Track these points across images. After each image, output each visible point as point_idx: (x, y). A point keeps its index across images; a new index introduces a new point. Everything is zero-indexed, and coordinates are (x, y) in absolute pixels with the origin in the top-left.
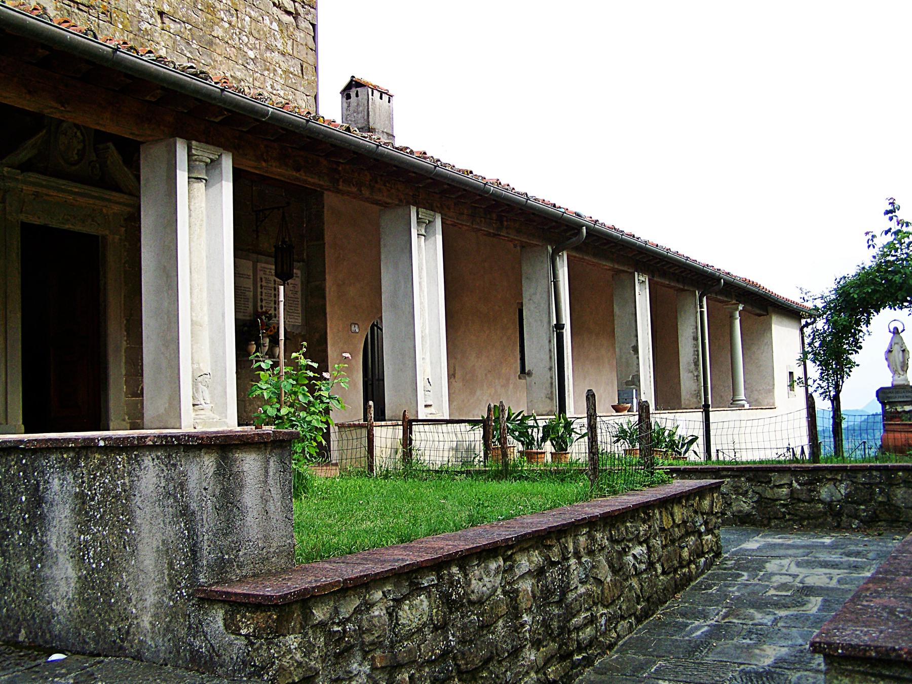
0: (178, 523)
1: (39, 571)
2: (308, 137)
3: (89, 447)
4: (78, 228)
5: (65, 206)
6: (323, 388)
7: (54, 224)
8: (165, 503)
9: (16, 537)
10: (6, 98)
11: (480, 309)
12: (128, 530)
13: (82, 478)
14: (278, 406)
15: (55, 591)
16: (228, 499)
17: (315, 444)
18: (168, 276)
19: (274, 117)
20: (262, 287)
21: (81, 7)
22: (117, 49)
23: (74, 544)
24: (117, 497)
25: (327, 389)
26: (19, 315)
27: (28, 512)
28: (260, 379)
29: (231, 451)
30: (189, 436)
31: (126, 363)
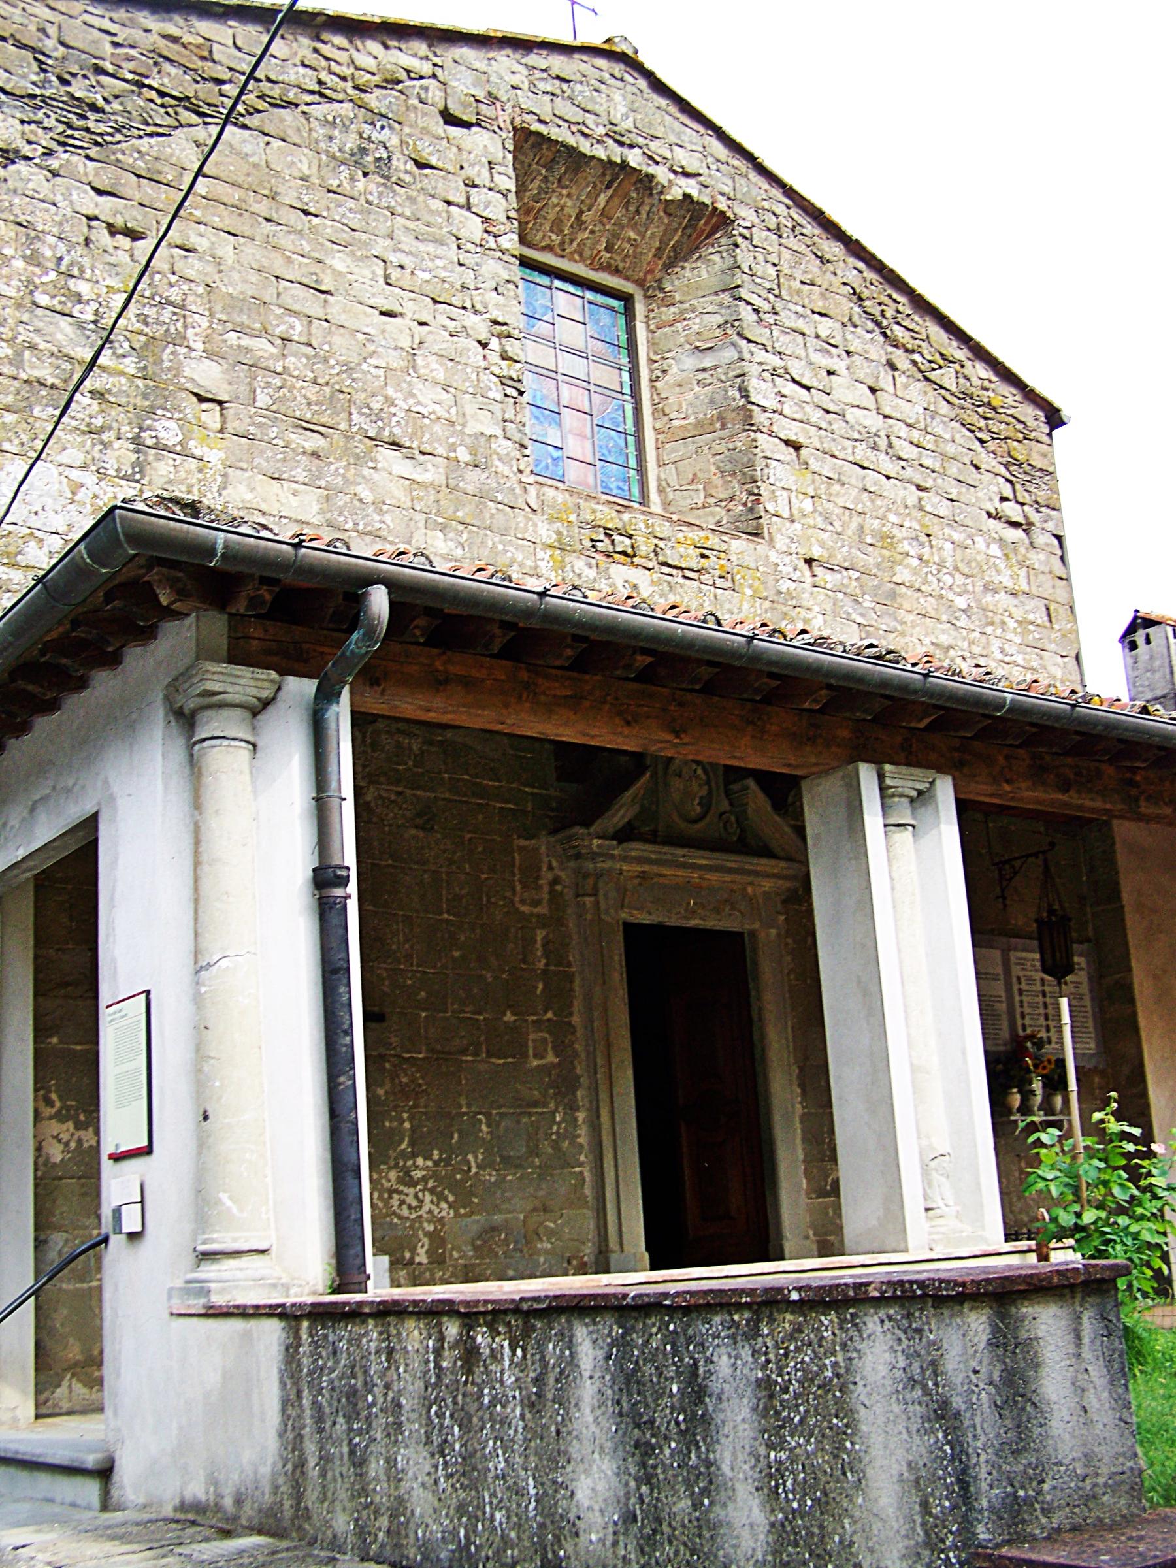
0: (933, 1431)
1: (707, 1511)
2: (1077, 733)
3: (770, 1302)
4: (711, 923)
5: (691, 890)
6: (1154, 1171)
7: (673, 921)
8: (908, 1396)
9: (667, 1452)
10: (593, 737)
12: (848, 1444)
13: (766, 1354)
14: (1077, 1208)
15: (735, 1546)
16: (1016, 1390)
17: (1149, 1273)
18: (866, 993)
19: (1016, 708)
20: (1021, 992)
21: (688, 573)
22: (752, 638)
23: (760, 1466)
24: (825, 1386)
25: (1163, 1174)
26: (630, 1073)
27: (683, 1410)
28: (1041, 1162)
29: (1013, 1303)
30: (941, 1281)
31: (804, 1140)
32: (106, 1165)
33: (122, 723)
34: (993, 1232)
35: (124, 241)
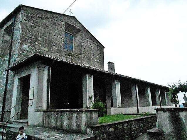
11: (126, 93)
32: (29, 100)
33: (34, 66)
34: (137, 113)
35: (34, 28)
